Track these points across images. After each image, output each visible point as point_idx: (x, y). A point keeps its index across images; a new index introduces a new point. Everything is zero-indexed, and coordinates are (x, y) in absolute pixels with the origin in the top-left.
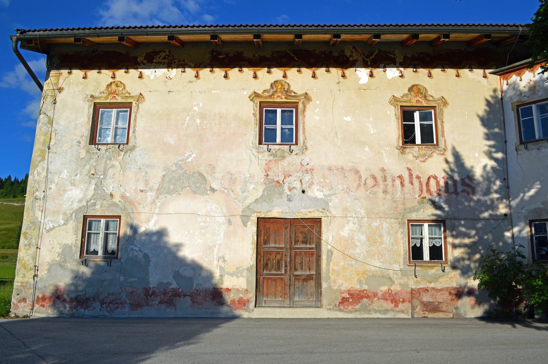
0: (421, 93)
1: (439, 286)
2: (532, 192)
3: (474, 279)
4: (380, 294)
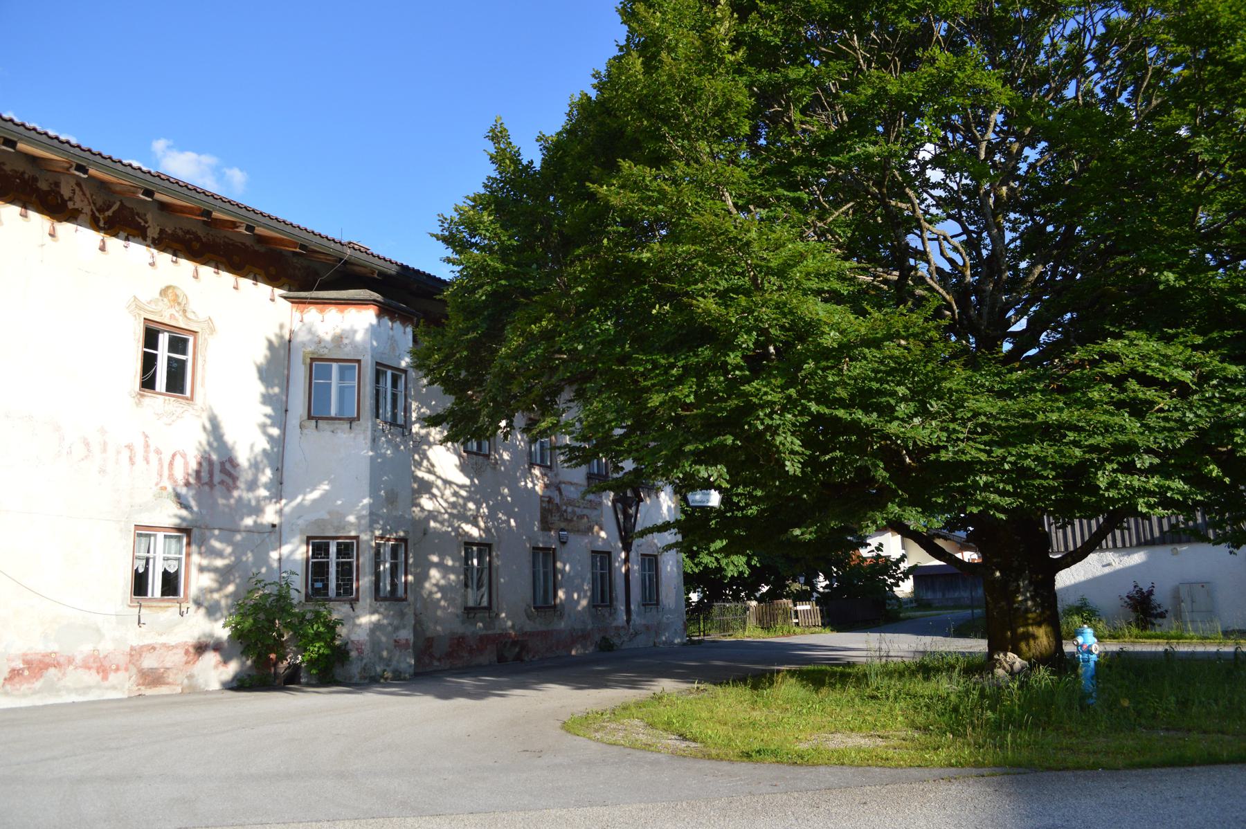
0: (179, 304)
1: (172, 640)
2: (316, 494)
3: (224, 626)
4: (79, 659)
